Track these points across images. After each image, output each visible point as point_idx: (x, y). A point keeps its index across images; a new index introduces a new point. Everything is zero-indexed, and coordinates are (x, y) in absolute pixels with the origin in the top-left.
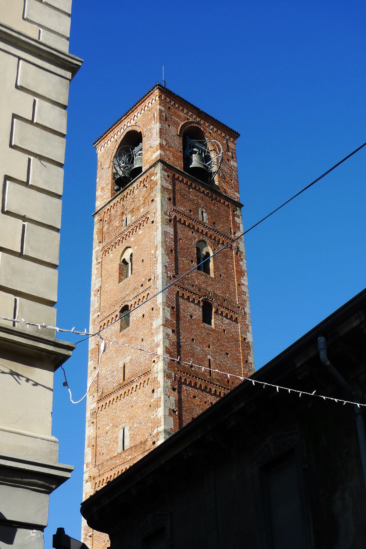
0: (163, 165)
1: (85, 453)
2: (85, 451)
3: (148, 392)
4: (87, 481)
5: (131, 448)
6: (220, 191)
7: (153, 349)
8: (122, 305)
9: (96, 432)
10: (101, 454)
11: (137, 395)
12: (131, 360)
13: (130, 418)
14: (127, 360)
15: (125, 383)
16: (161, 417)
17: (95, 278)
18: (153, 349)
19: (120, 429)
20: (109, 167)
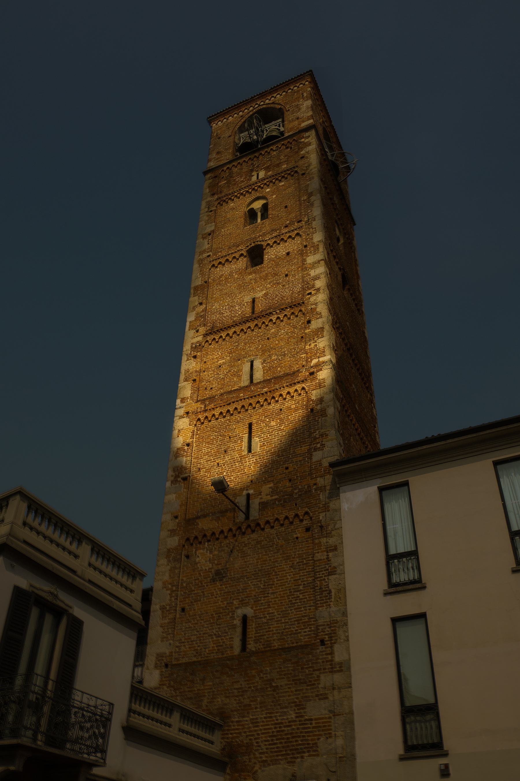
0: (317, 147)
1: (179, 388)
2: (179, 385)
3: (299, 324)
4: (182, 417)
5: (266, 382)
6: (303, 643)
7: (249, 599)
8: (250, 245)
9: (198, 395)
10: (209, 388)
11: (278, 327)
12: (266, 295)
13: (264, 351)
14: (259, 295)
15: (254, 316)
16: (324, 347)
17: (204, 224)
18: (249, 599)
19: (245, 362)
20: (231, 136)
